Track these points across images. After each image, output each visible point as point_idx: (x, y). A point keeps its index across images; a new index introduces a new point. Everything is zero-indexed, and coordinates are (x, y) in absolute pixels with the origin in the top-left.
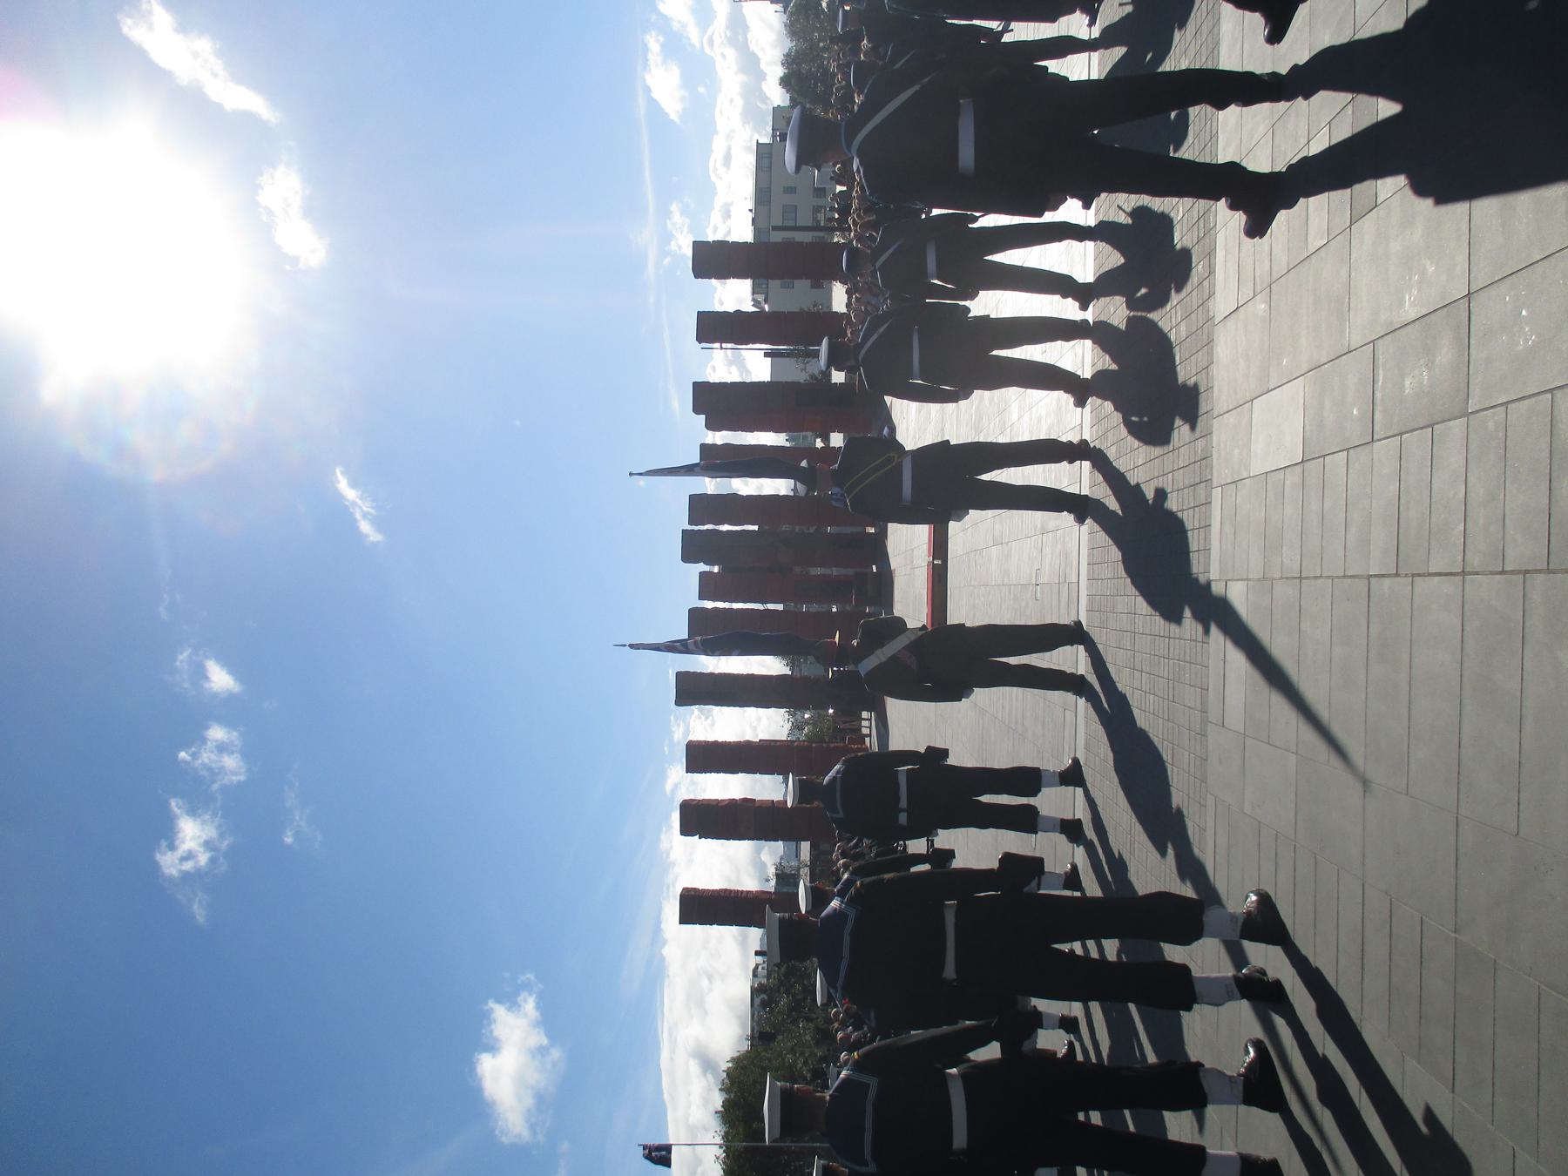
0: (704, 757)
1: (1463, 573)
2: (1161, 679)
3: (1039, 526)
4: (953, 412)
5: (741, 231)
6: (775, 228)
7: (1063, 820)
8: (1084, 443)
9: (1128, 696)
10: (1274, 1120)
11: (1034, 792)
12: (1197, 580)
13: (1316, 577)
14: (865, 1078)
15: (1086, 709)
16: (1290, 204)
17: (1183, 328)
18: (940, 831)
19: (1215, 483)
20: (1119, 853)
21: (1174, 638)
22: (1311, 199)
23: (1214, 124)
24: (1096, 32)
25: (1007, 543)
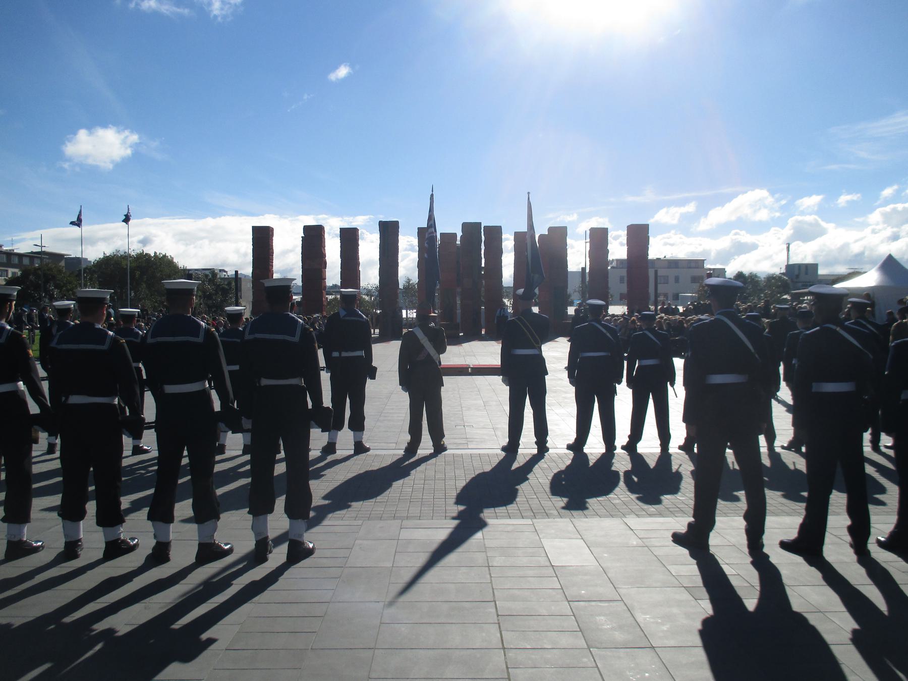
0: (349, 238)
1: (504, 648)
3: (497, 426)
4: (556, 377)
5: (657, 250)
6: (656, 272)
7: (335, 444)
8: (547, 450)
9: (409, 477)
10: (192, 559)
13: (490, 574)
14: (202, 334)
15: (399, 455)
16: (693, 555)
17: (617, 501)
18: (329, 374)
19: (535, 520)
20: (325, 475)
21: (445, 501)
22: (696, 567)
23: (732, 515)
24: (778, 450)
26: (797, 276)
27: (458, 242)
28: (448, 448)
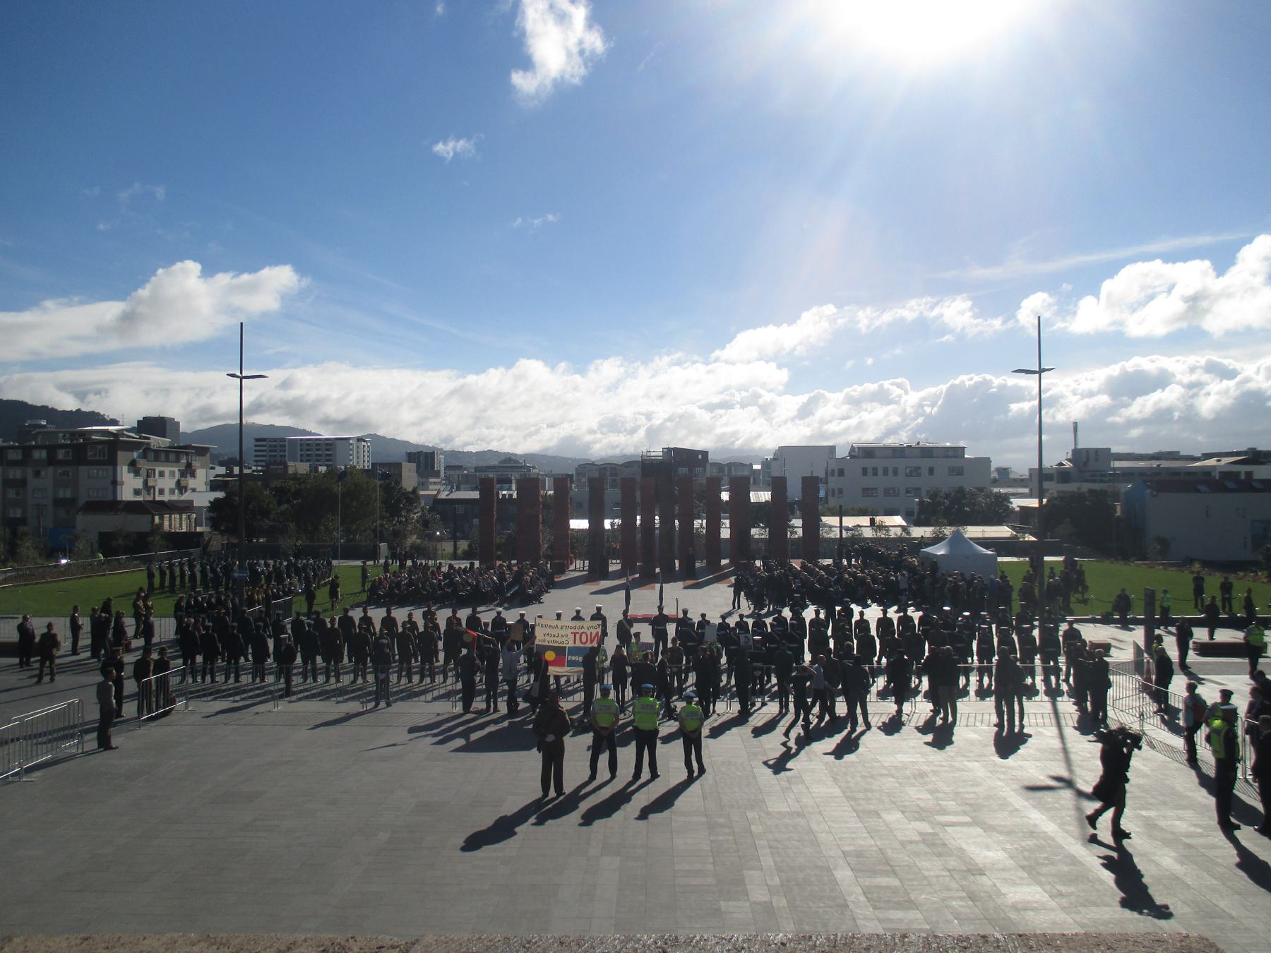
26: (1085, 464)
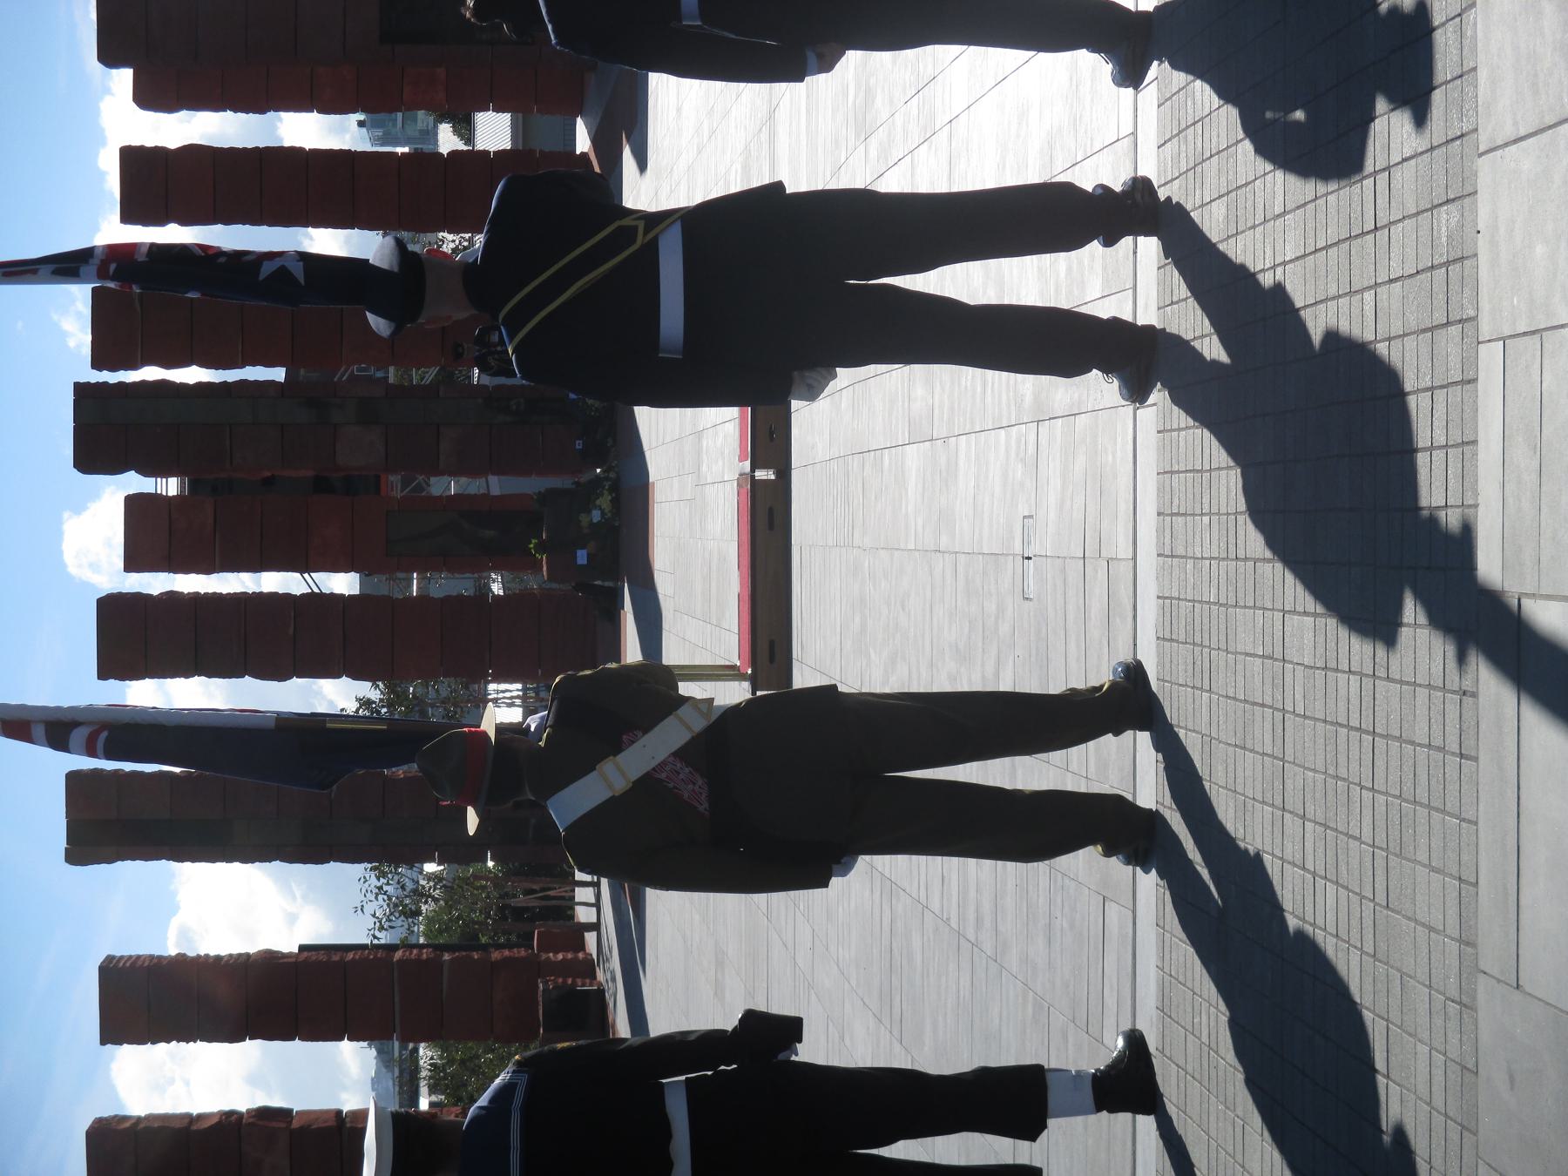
2: (1353, 844)
8: (1141, 186)
11: (1030, 1128)
12: (1433, 521)
19: (1486, 330)
25: (945, 439)
27: (171, 487)
28: (1130, 659)
